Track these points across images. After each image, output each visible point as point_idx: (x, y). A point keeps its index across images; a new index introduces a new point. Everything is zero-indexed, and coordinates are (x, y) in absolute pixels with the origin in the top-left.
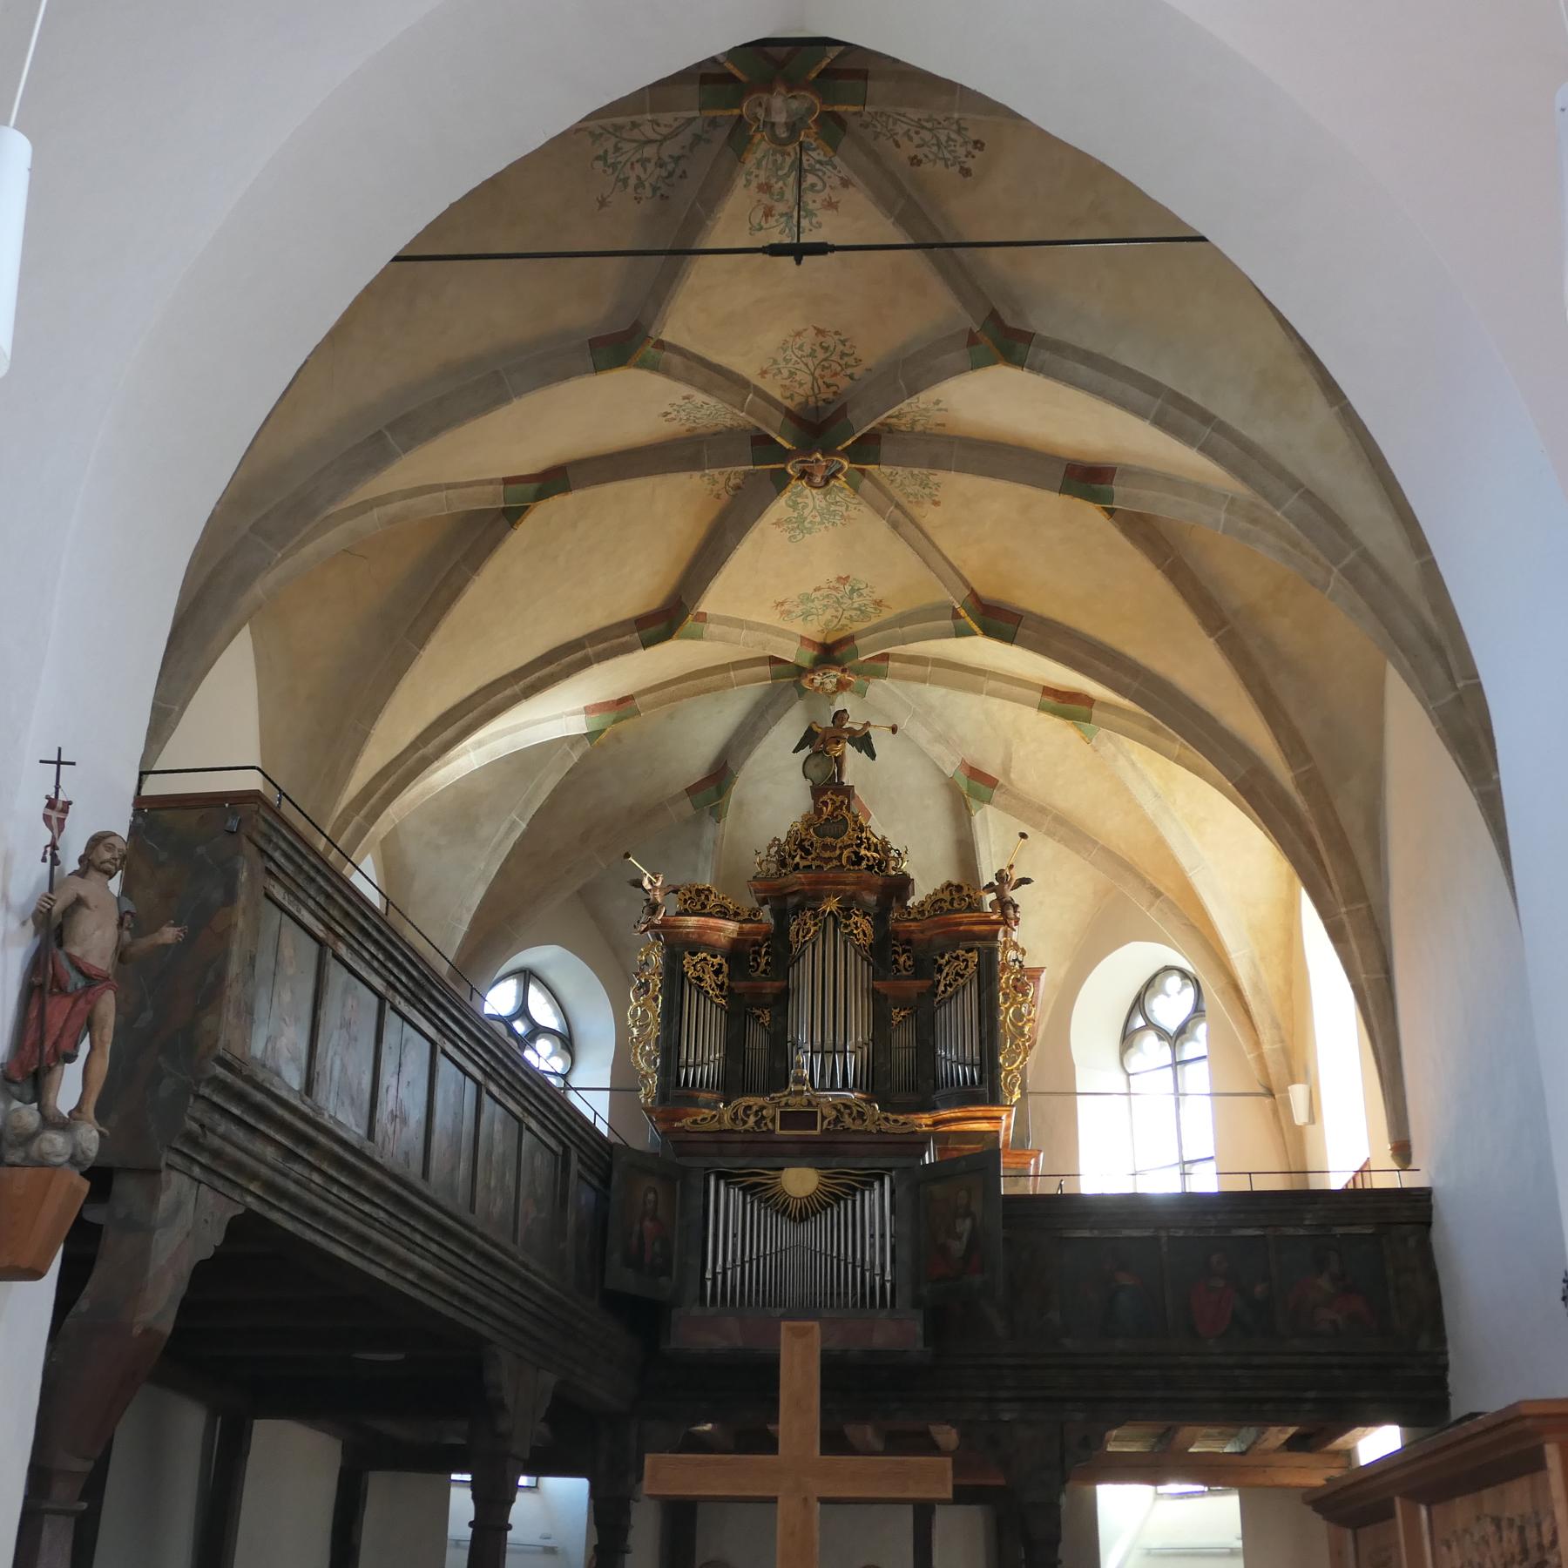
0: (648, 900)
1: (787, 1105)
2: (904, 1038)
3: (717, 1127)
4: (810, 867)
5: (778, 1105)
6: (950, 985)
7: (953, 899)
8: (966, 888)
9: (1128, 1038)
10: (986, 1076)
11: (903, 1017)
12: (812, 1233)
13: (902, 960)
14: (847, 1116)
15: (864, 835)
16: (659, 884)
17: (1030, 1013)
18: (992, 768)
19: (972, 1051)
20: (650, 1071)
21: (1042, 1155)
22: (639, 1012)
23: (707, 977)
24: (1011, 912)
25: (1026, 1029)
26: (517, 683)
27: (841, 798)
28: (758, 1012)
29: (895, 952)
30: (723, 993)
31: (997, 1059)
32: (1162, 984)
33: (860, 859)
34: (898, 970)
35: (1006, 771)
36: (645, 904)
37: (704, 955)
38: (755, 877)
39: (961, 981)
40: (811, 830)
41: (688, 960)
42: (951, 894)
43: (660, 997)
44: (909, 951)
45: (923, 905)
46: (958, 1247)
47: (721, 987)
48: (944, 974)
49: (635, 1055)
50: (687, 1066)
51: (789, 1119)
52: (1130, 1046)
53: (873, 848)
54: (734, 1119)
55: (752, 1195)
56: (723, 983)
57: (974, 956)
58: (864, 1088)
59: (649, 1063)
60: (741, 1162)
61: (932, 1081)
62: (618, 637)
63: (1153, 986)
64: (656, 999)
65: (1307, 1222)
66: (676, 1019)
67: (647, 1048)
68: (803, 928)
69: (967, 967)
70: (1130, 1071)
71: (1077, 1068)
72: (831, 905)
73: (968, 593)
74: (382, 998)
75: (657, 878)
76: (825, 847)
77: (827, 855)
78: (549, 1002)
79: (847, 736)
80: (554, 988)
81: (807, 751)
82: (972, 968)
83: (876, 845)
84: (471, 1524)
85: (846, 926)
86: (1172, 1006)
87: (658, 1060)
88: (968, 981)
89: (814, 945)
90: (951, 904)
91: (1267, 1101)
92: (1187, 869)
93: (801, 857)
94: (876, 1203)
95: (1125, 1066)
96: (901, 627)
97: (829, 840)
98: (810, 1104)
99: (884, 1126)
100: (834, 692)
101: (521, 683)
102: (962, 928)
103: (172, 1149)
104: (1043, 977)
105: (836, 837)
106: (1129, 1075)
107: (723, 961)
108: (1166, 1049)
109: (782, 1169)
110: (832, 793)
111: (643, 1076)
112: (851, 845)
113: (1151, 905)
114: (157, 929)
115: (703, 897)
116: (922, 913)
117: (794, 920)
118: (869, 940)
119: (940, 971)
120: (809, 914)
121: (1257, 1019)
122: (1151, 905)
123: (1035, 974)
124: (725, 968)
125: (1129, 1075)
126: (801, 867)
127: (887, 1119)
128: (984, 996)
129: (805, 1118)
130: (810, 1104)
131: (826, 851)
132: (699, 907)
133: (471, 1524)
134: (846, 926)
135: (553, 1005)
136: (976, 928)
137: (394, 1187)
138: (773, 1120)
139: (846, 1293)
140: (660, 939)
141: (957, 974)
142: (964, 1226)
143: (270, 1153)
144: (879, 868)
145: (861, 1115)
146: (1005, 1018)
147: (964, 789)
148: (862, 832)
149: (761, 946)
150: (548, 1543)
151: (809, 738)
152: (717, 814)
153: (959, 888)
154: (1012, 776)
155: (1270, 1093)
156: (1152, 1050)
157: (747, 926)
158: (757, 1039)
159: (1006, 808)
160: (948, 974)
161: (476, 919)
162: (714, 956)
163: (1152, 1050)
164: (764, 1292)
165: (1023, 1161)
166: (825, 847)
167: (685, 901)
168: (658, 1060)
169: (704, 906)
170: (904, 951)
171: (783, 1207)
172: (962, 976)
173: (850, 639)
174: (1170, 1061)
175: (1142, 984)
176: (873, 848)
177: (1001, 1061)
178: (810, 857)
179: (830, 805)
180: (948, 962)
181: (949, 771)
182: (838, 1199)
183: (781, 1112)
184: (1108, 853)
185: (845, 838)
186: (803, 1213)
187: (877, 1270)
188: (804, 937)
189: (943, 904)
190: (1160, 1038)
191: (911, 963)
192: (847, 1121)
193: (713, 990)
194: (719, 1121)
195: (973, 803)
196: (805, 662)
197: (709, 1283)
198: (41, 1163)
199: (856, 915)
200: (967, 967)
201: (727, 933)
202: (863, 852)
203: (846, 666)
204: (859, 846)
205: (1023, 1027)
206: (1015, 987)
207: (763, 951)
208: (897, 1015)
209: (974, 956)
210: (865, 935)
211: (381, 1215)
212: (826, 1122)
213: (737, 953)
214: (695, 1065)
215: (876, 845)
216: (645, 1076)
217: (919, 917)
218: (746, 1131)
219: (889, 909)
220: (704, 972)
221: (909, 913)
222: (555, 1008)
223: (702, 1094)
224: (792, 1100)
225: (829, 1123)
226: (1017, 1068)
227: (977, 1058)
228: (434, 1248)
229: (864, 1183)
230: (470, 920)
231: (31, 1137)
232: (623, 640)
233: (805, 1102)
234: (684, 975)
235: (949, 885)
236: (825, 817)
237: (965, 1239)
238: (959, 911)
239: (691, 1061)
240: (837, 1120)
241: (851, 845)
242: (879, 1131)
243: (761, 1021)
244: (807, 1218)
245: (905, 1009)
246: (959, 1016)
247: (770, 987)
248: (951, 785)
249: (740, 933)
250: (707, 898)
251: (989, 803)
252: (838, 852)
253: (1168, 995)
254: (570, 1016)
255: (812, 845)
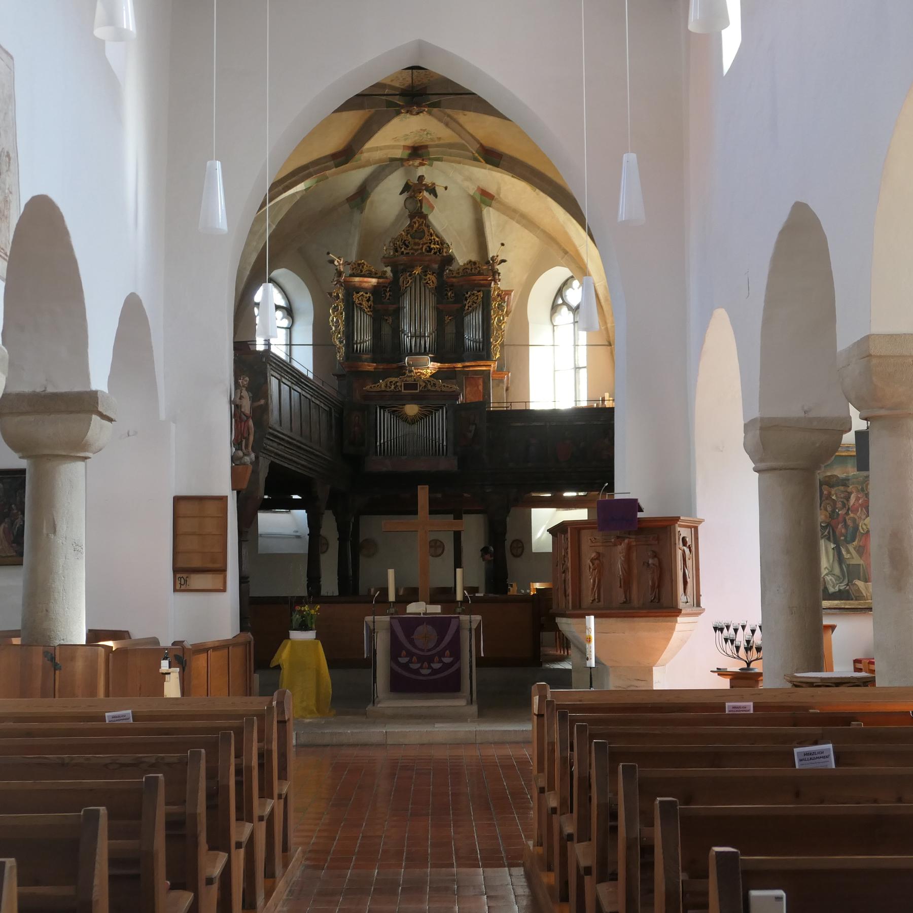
0: (337, 269)
1: (406, 381)
2: (450, 329)
3: (379, 389)
4: (408, 253)
5: (403, 381)
6: (471, 307)
7: (472, 269)
8: (478, 263)
9: (554, 308)
10: (485, 347)
11: (450, 320)
12: (415, 428)
13: (449, 294)
14: (429, 385)
15: (432, 238)
16: (341, 262)
17: (503, 319)
18: (492, 190)
19: (479, 336)
20: (341, 346)
21: (510, 374)
22: (335, 320)
23: (364, 303)
24: (497, 276)
25: (503, 327)
26: (280, 185)
27: (422, 220)
28: (386, 318)
29: (447, 290)
30: (371, 310)
31: (490, 340)
32: (571, 284)
33: (431, 249)
34: (448, 299)
35: (499, 194)
36: (336, 272)
37: (362, 293)
38: (384, 257)
39: (475, 305)
40: (409, 235)
41: (355, 296)
42: (471, 266)
43: (344, 313)
44: (452, 289)
45: (459, 270)
46: (470, 435)
47: (370, 307)
48: (468, 302)
49: (334, 339)
50: (357, 343)
51: (407, 386)
52: (555, 312)
53: (436, 243)
54: (386, 386)
55: (393, 415)
56: (371, 305)
57: (481, 294)
58: (433, 351)
59: (341, 342)
60: (389, 402)
61: (462, 348)
62: (324, 163)
63: (566, 284)
64: (342, 314)
65: (601, 419)
66: (351, 323)
67: (339, 336)
68: (405, 280)
69: (478, 298)
70: (555, 324)
71: (530, 324)
72: (418, 271)
73: (478, 146)
74: (290, 387)
75: (341, 260)
76: (415, 244)
77: (416, 247)
78: (280, 292)
79: (424, 188)
80: (283, 287)
81: (405, 195)
82: (480, 300)
83: (438, 242)
84: (308, 535)
85: (425, 279)
86: (574, 295)
87: (344, 341)
88: (478, 305)
89: (411, 288)
90: (471, 270)
91: (609, 348)
92: (578, 246)
93: (405, 249)
94: (440, 418)
95: (553, 321)
96: (449, 149)
97: (417, 240)
98: (415, 381)
99: (444, 389)
100: (418, 166)
101: (282, 185)
102: (476, 282)
103: (262, 452)
104: (513, 294)
105: (421, 239)
106: (554, 326)
107: (371, 295)
108: (571, 314)
109: (405, 405)
110: (418, 218)
111: (338, 348)
112: (427, 243)
113: (562, 258)
114: (259, 400)
115: (361, 267)
116: (458, 273)
117: (402, 276)
118: (435, 284)
119: (466, 300)
120: (408, 274)
121: (606, 313)
122: (562, 258)
123: (508, 293)
124: (372, 298)
125: (554, 326)
126: (405, 253)
127: (444, 386)
128: (485, 312)
129: (414, 386)
130: (415, 381)
131: (415, 245)
132: (359, 272)
133: (308, 535)
134: (425, 279)
135: (282, 294)
136: (482, 282)
137: (287, 438)
138: (401, 386)
139: (429, 450)
140: (342, 286)
141: (473, 302)
142: (473, 428)
143: (275, 445)
144: (439, 253)
145: (434, 384)
146: (494, 322)
147: (479, 200)
148: (432, 236)
149: (387, 287)
150: (298, 534)
151: (407, 188)
152: (362, 210)
153: (475, 263)
154: (501, 196)
155: (610, 345)
156: (565, 316)
157: (381, 280)
158: (386, 330)
159: (498, 210)
160: (469, 302)
161: (252, 270)
162: (367, 293)
163: (565, 316)
164: (427, 450)
165: (501, 376)
166: (415, 244)
167: (353, 269)
168: (344, 341)
169: (361, 271)
170: (451, 290)
171: (405, 419)
172: (476, 303)
173: (426, 147)
174: (572, 321)
175: (562, 283)
176: (436, 243)
177: (492, 340)
178: (408, 249)
179: (417, 224)
180: (470, 296)
181: (472, 193)
182: (426, 416)
183: (404, 384)
184: (544, 232)
185: (424, 239)
186: (413, 421)
187: (441, 442)
188: (406, 284)
189: (467, 270)
190: (569, 310)
191: (453, 295)
192: (429, 387)
193: (367, 309)
194: (380, 387)
195: (483, 206)
196: (405, 156)
197: (378, 447)
198: (245, 464)
199: (429, 274)
200: (478, 298)
201: (372, 284)
202: (432, 246)
203: (424, 158)
204: (430, 243)
205: (501, 325)
206: (498, 308)
207: (388, 289)
208: (447, 319)
209: (481, 294)
210: (433, 283)
211: (294, 452)
212: (421, 387)
213: (376, 290)
214: (360, 343)
215: (438, 242)
216: (339, 348)
217: (457, 275)
218: (391, 391)
219: (444, 271)
220: (362, 301)
221: (453, 274)
222: (279, 290)
223: (364, 356)
224: (408, 379)
225: (422, 388)
226: (498, 344)
227: (481, 340)
228: (304, 457)
229: (436, 410)
230: (250, 269)
231: (241, 458)
232: (326, 164)
233: (413, 380)
234: (354, 303)
235: (470, 261)
236: (414, 229)
237: (473, 432)
238: (474, 275)
239: (358, 341)
240: (425, 386)
241: (427, 243)
242: (441, 391)
243: (388, 322)
244: (414, 423)
245: (451, 316)
246: (475, 319)
247: (392, 308)
248: (473, 198)
249: (378, 283)
250: (363, 267)
251: (490, 206)
252: (421, 246)
253: (574, 289)
254: (291, 301)
255: (409, 243)
